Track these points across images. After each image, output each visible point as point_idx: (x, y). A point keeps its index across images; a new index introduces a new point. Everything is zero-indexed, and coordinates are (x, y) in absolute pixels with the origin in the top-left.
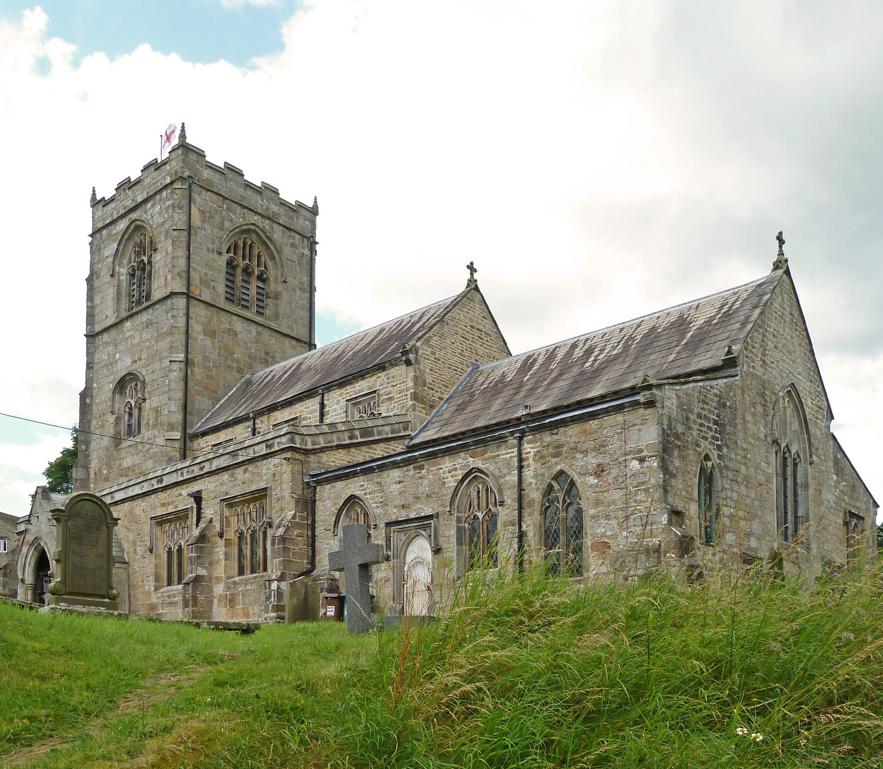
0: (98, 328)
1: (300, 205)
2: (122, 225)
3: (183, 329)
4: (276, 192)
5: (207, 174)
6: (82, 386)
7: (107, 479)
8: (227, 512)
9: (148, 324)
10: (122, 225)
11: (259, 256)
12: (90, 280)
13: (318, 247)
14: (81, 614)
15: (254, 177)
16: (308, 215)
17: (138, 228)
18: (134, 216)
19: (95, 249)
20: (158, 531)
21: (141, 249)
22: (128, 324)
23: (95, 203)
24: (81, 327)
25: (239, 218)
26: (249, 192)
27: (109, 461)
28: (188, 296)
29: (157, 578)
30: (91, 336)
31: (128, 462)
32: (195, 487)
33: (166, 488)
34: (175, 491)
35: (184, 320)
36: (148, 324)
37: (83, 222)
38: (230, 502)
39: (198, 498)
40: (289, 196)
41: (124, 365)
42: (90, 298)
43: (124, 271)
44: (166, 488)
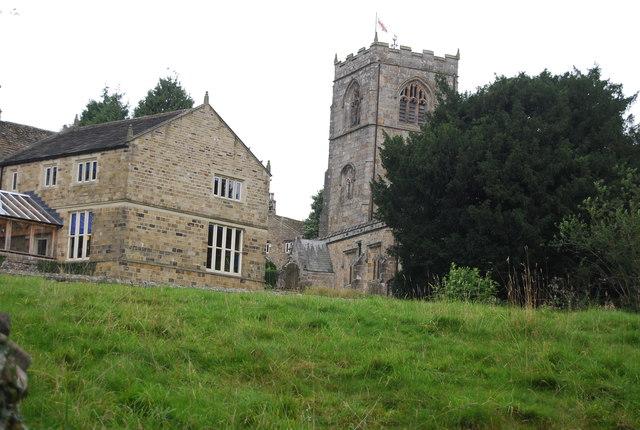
0: (336, 136)
1: (447, 57)
2: (348, 80)
3: (373, 144)
4: (431, 53)
5: (389, 56)
6: (326, 168)
7: (336, 222)
8: (369, 251)
9: (358, 139)
10: (348, 80)
11: (421, 93)
12: (332, 107)
13: (459, 80)
14: (73, 281)
15: (417, 49)
16: (452, 61)
17: (355, 83)
18: (354, 76)
19: (335, 91)
20: (346, 257)
21: (357, 94)
22: (349, 136)
23: (337, 64)
24: (327, 135)
25: (408, 75)
26: (415, 59)
27: (338, 211)
28: (377, 125)
29: (345, 280)
30: (332, 140)
31: (346, 214)
32: (359, 238)
33: (349, 238)
34: (352, 240)
35: (373, 138)
36: (358, 139)
37: (330, 74)
38: (370, 246)
39: (360, 245)
40: (440, 53)
41: (346, 159)
42: (332, 118)
43: (348, 105)
44: (349, 238)
